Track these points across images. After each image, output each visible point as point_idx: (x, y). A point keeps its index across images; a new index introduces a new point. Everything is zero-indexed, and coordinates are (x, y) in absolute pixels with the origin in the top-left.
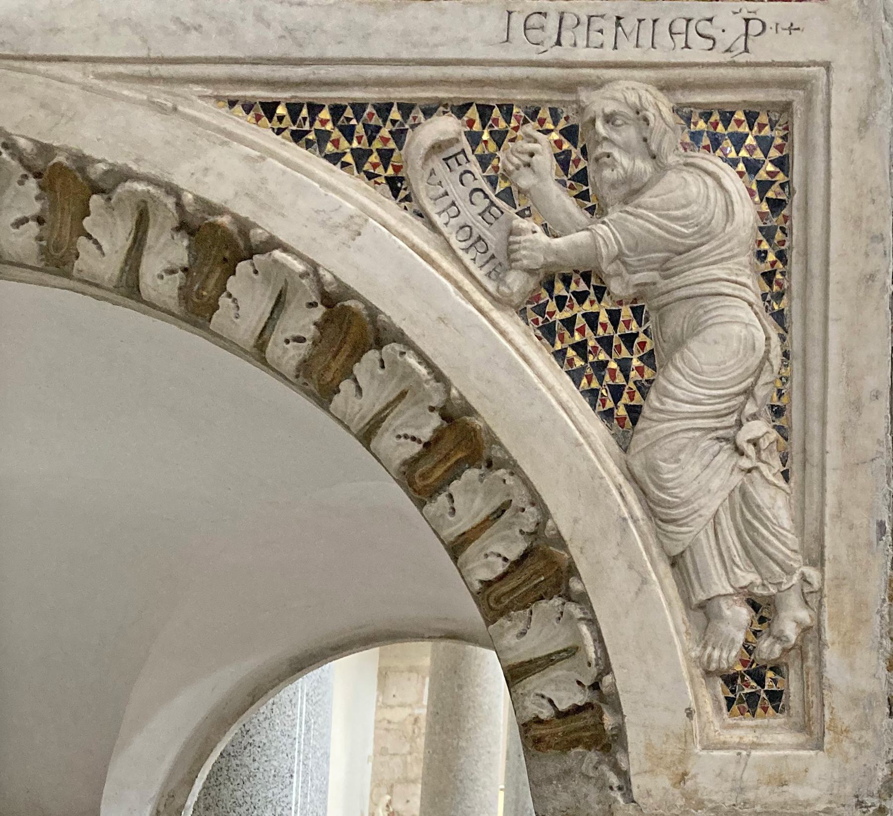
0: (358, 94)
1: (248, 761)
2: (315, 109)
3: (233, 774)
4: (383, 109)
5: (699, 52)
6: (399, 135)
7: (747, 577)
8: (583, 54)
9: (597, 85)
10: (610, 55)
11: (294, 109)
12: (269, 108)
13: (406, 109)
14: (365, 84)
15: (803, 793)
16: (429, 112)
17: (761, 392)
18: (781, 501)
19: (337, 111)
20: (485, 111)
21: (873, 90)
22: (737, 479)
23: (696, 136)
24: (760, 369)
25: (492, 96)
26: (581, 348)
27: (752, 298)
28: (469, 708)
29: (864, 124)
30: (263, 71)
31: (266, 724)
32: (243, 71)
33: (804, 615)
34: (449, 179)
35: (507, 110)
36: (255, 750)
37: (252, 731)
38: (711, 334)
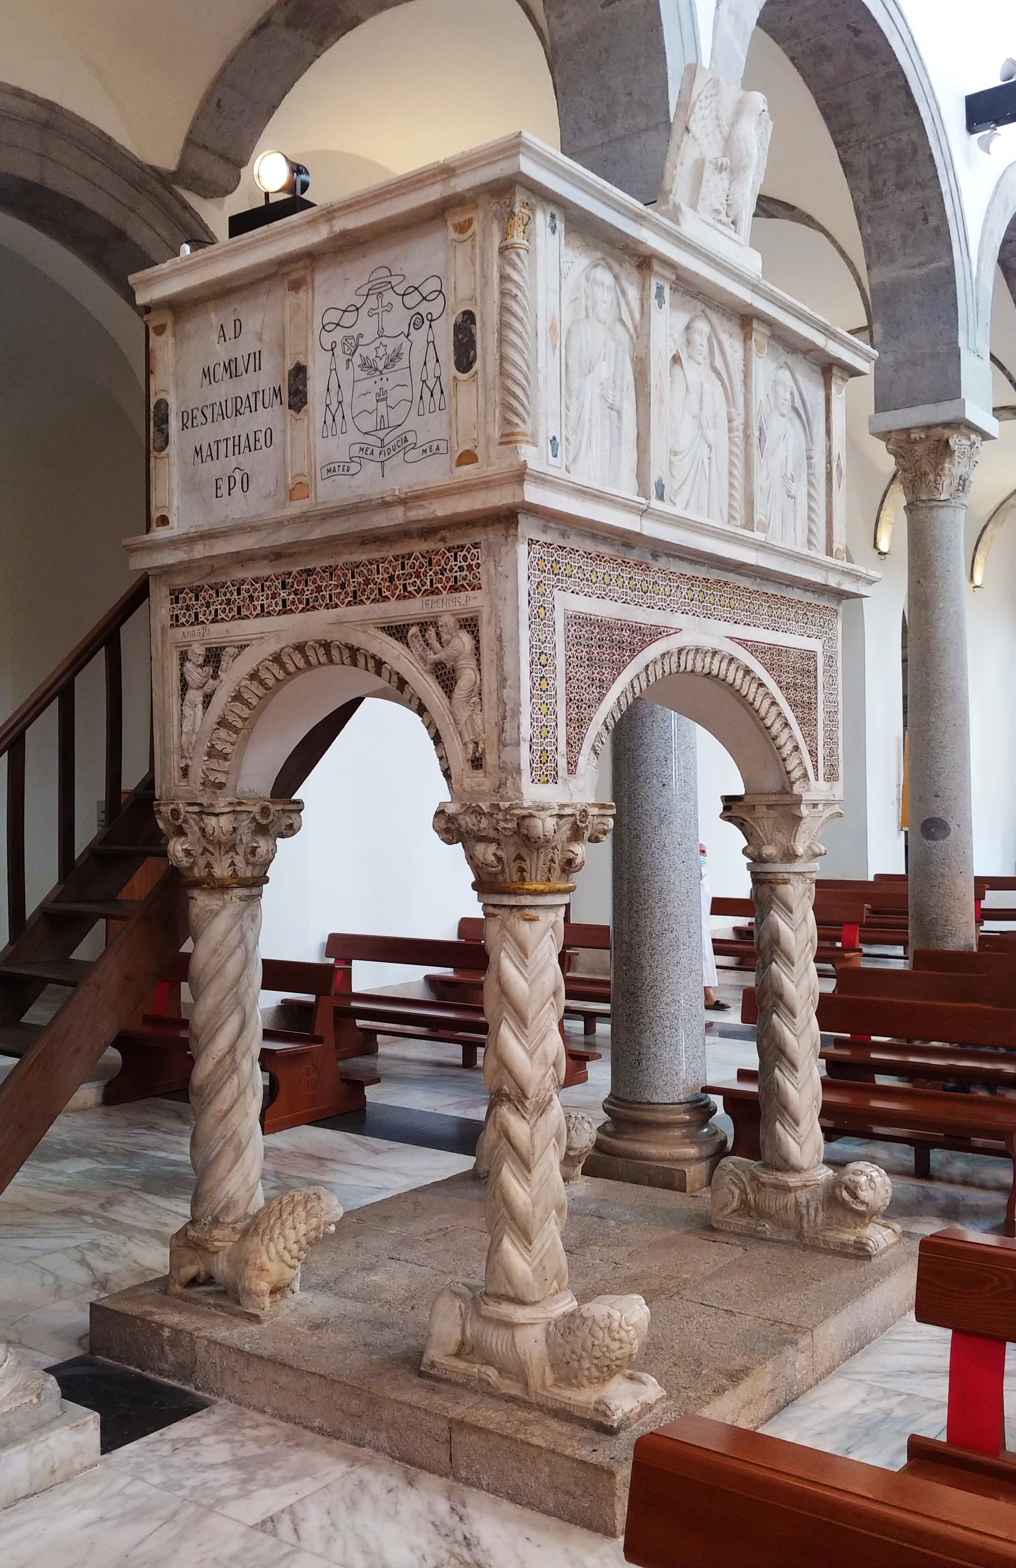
0: (399, 623)
1: (642, 753)
2: (392, 627)
3: (635, 761)
4: (404, 625)
5: (458, 607)
6: (407, 632)
7: (472, 737)
8: (437, 610)
9: (440, 616)
10: (442, 609)
11: (388, 627)
12: (384, 627)
13: (408, 625)
14: (399, 621)
15: (482, 788)
16: (412, 625)
17: (475, 690)
18: (479, 717)
19: (396, 627)
20: (422, 623)
21: (491, 612)
22: (470, 713)
23: (461, 626)
24: (474, 685)
25: (422, 621)
26: (443, 680)
27: (472, 666)
28: (935, 691)
29: (490, 622)
30: (381, 621)
31: (650, 733)
32: (378, 621)
33: (482, 746)
34: (416, 641)
35: (426, 623)
36: (645, 747)
37: (643, 737)
38: (463, 678)
